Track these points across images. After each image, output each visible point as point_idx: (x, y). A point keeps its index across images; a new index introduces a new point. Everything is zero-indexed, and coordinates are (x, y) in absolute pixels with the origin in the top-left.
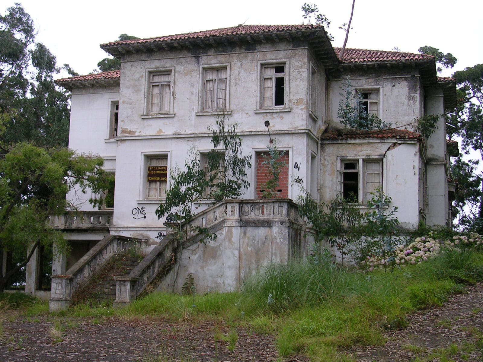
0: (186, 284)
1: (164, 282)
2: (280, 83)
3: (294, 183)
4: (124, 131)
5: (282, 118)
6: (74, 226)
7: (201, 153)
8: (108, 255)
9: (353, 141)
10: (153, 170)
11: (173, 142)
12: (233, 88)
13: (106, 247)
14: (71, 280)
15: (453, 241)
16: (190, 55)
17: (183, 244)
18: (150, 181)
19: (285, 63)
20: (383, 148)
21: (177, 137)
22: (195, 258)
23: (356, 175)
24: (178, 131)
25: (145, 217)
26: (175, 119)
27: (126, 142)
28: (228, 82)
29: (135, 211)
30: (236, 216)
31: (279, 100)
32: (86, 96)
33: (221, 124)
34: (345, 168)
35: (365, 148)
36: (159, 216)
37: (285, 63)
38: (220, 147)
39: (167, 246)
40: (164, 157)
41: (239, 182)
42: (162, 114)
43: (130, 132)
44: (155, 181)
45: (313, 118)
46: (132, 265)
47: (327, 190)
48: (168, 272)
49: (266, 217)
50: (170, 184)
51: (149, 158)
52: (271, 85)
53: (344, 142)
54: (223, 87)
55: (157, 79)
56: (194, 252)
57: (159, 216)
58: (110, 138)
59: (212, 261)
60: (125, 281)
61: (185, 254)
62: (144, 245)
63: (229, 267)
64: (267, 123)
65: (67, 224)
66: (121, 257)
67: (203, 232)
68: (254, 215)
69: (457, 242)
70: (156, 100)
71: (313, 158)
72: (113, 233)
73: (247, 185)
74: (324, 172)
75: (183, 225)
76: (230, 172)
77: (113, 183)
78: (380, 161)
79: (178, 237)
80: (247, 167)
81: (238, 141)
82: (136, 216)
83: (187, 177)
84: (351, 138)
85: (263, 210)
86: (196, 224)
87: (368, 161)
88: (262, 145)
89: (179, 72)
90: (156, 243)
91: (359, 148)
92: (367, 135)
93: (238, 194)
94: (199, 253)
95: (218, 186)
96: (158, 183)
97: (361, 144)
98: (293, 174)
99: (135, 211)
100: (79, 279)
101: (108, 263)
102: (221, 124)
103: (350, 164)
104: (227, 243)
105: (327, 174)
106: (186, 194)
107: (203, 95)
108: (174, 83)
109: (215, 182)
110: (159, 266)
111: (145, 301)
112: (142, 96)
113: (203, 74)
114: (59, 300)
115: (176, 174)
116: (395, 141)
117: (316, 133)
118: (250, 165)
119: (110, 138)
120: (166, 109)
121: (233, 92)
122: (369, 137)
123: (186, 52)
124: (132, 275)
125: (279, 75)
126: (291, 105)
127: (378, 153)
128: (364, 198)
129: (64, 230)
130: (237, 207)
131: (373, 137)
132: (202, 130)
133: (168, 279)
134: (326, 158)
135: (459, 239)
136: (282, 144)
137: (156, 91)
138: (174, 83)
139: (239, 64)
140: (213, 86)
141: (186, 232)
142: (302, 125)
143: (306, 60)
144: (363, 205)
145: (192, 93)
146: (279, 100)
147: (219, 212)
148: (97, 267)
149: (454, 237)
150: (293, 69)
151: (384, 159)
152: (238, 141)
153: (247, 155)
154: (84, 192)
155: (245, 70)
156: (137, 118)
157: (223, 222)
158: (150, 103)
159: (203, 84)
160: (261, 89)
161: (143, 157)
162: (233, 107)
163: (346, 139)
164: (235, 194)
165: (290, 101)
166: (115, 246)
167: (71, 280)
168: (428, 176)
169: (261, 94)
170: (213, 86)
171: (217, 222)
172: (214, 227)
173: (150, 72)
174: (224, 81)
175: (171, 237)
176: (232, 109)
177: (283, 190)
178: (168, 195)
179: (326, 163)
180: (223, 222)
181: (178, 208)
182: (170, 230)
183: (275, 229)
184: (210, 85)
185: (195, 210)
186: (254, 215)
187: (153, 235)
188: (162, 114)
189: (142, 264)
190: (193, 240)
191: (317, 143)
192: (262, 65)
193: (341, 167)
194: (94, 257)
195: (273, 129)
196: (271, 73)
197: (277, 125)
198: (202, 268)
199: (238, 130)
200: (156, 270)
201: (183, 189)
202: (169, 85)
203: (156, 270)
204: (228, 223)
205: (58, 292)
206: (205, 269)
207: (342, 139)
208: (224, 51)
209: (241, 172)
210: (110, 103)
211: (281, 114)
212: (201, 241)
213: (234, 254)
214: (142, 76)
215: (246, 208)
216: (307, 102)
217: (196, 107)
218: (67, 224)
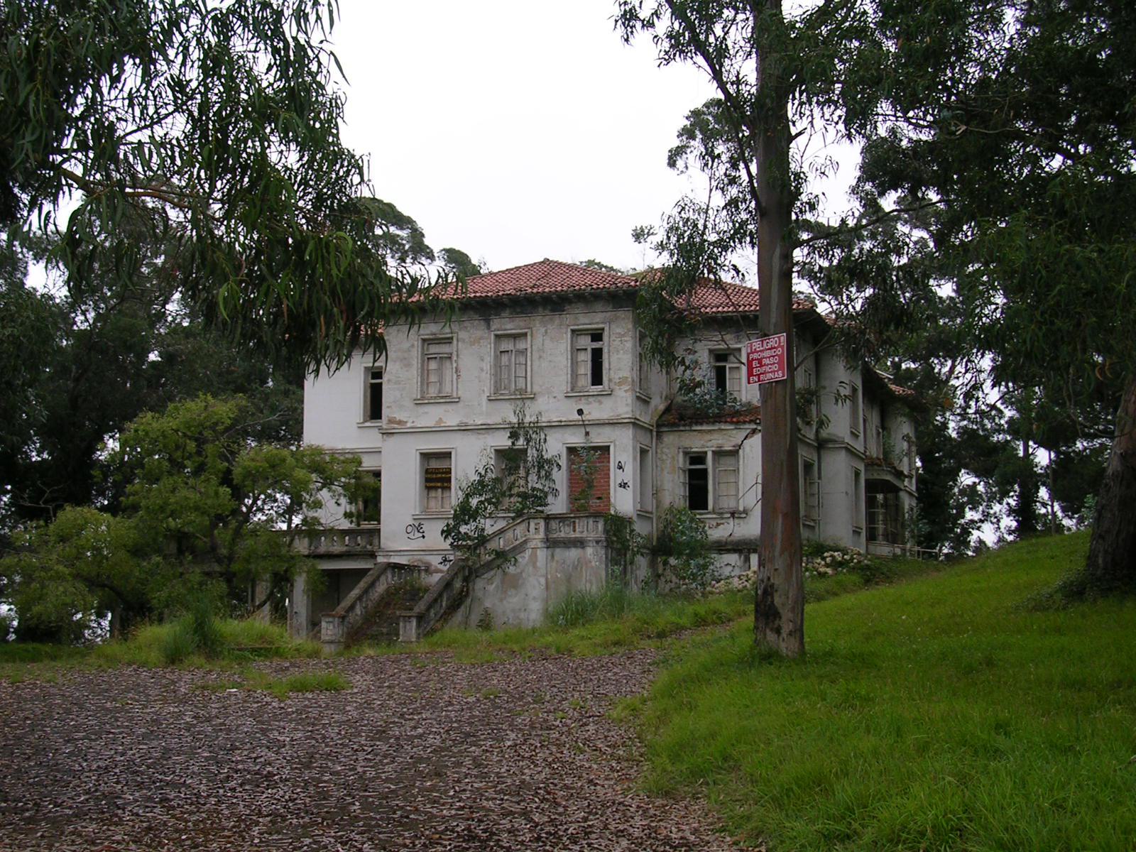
0: (481, 621)
1: (454, 619)
2: (597, 356)
3: (618, 488)
4: (391, 421)
5: (600, 403)
6: (322, 549)
7: (496, 450)
8: (381, 588)
9: (699, 428)
10: (432, 473)
11: (459, 435)
12: (536, 363)
13: (378, 577)
14: (343, 618)
15: (824, 559)
16: (477, 317)
17: (476, 571)
18: (429, 488)
19: (603, 329)
20: (738, 436)
21: (464, 429)
22: (491, 588)
23: (705, 471)
24: (465, 420)
25: (423, 537)
26: (460, 405)
27: (395, 436)
28: (529, 354)
29: (409, 529)
30: (542, 535)
31: (597, 378)
32: (365, 407)
33: (520, 413)
34: (691, 464)
35: (716, 436)
36: (445, 538)
37: (603, 329)
38: (521, 442)
39: (456, 574)
40: (447, 455)
41: (546, 489)
42: (442, 397)
43: (400, 422)
44: (436, 488)
45: (643, 400)
46: (413, 600)
47: (667, 493)
48: (459, 606)
49: (578, 535)
50: (455, 497)
51: (426, 456)
52: (586, 357)
53: (687, 428)
54: (522, 360)
55: (434, 349)
56: (490, 581)
57: (445, 538)
58: (365, 421)
59: (512, 592)
60: (409, 617)
61: (479, 584)
62: (423, 574)
63: (534, 598)
64: (580, 412)
65: (312, 548)
66: (397, 590)
67: (502, 556)
68: (565, 532)
69: (828, 560)
70: (433, 378)
71: (643, 452)
72: (380, 560)
73: (555, 492)
74: (662, 469)
75: (476, 547)
76: (533, 478)
77: (377, 492)
78: (734, 453)
79: (470, 563)
80: (556, 469)
81: (543, 436)
82: (411, 536)
83: (479, 486)
84: (696, 424)
85: (574, 527)
86: (492, 545)
87: (719, 454)
88: (576, 438)
89: (464, 341)
90: (441, 571)
91: (708, 437)
92: (718, 419)
93: (546, 505)
94: (497, 581)
95: (519, 495)
96: (440, 490)
97: (710, 431)
98: (615, 477)
99: (409, 529)
100: (351, 618)
101: (382, 598)
102: (520, 413)
103: (698, 458)
104: (531, 568)
105: (665, 472)
106: (477, 508)
107: (496, 372)
108: (457, 356)
109: (515, 491)
110: (448, 599)
111: (436, 637)
112: (414, 373)
113: (495, 345)
114: (332, 642)
115: (464, 485)
116: (755, 426)
117: (647, 418)
118: (559, 466)
119: (365, 421)
120: (447, 389)
121: (535, 368)
122: (720, 422)
123: (472, 313)
124: (417, 610)
125: (597, 345)
126: (612, 386)
127: (733, 444)
128: (715, 503)
129: (308, 556)
130: (542, 523)
131: (726, 422)
132: (494, 419)
133: (459, 616)
134: (665, 450)
135: (831, 556)
136: (599, 437)
137: (433, 365)
138: (457, 356)
139: (543, 330)
140: (510, 360)
141: (479, 556)
142: (627, 413)
143: (630, 326)
144: (714, 512)
145: (482, 370)
146: (597, 378)
147: (520, 530)
148: (369, 603)
149: (826, 554)
150: (613, 338)
151: (741, 451)
152: (543, 436)
153: (556, 454)
154: (339, 505)
155: (551, 338)
156: (408, 403)
157: (525, 542)
158: (425, 382)
159: (496, 357)
160: (572, 363)
161: (418, 457)
162: (536, 389)
163: (690, 425)
164: (541, 506)
165: (610, 380)
166: (390, 576)
167: (343, 618)
168: (823, 465)
169: (572, 371)
170: (510, 360)
171: (518, 542)
172: (515, 548)
173: (424, 340)
174: (524, 352)
175: (461, 563)
176: (534, 390)
177: (604, 497)
178: (456, 511)
179: (664, 457)
180: (525, 542)
181: (468, 527)
182: (459, 553)
183: (589, 551)
184: (505, 358)
185: (489, 527)
186: (565, 532)
187: (435, 561)
188: (442, 397)
189: (428, 598)
190: (488, 566)
191: (651, 431)
192: (573, 331)
193: (685, 462)
194: (366, 591)
195: (588, 417)
196: (585, 342)
197: (595, 411)
198: (501, 600)
199: (544, 419)
200: (444, 604)
201: (474, 502)
202: (450, 358)
203: (444, 604)
204: (531, 544)
205: (329, 633)
206: (505, 602)
207: (684, 425)
208: (523, 313)
209: (548, 476)
210: (363, 369)
211: (599, 398)
212: (499, 567)
213: (539, 583)
214: (413, 346)
215: (554, 524)
216: (633, 381)
217: (487, 389)
218: (312, 548)
